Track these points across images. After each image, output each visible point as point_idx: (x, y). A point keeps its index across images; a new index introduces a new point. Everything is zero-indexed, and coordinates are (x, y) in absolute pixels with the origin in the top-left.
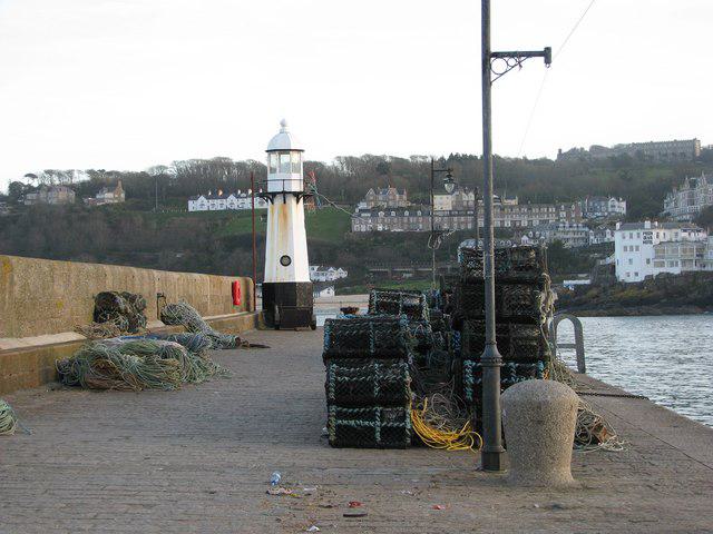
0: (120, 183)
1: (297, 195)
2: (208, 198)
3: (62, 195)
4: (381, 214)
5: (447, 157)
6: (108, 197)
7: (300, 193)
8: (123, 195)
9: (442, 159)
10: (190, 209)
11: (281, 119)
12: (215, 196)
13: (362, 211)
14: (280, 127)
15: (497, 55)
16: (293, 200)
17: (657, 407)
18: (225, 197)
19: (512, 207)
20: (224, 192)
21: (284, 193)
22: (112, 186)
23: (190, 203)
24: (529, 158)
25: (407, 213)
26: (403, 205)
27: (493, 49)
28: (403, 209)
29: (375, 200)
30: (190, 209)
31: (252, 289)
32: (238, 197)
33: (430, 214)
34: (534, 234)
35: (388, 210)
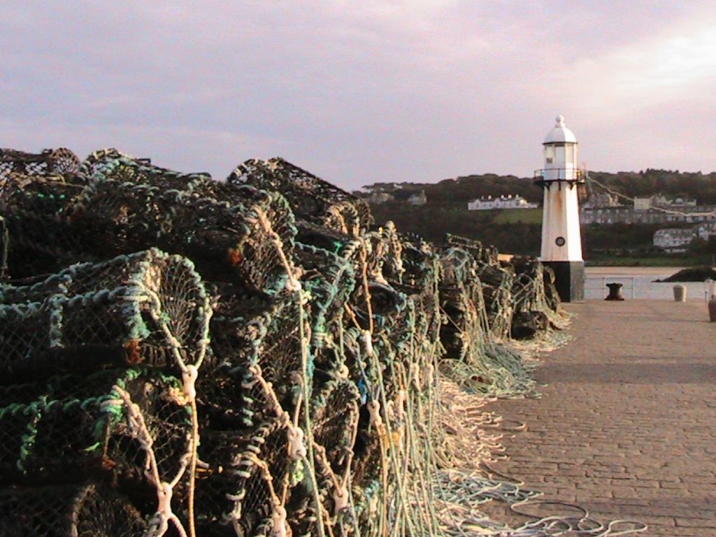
0: (423, 191)
1: (571, 183)
2: (482, 201)
3: (386, 197)
4: (600, 212)
5: (644, 171)
6: (416, 200)
7: (573, 181)
8: (425, 199)
9: (641, 172)
10: (470, 208)
11: (555, 117)
12: (486, 199)
13: (586, 209)
14: (556, 123)
15: (560, 185)
16: (567, 189)
17: (526, 209)
18: (493, 200)
19: (692, 208)
20: (493, 197)
21: (559, 181)
22: (417, 193)
23: (470, 204)
24: (681, 172)
25: (617, 211)
26: (614, 205)
27: (562, 182)
28: (615, 208)
29: (596, 202)
30: (470, 208)
31: (487, 321)
32: (502, 200)
33: (632, 211)
34: (708, 225)
35: (605, 209)
